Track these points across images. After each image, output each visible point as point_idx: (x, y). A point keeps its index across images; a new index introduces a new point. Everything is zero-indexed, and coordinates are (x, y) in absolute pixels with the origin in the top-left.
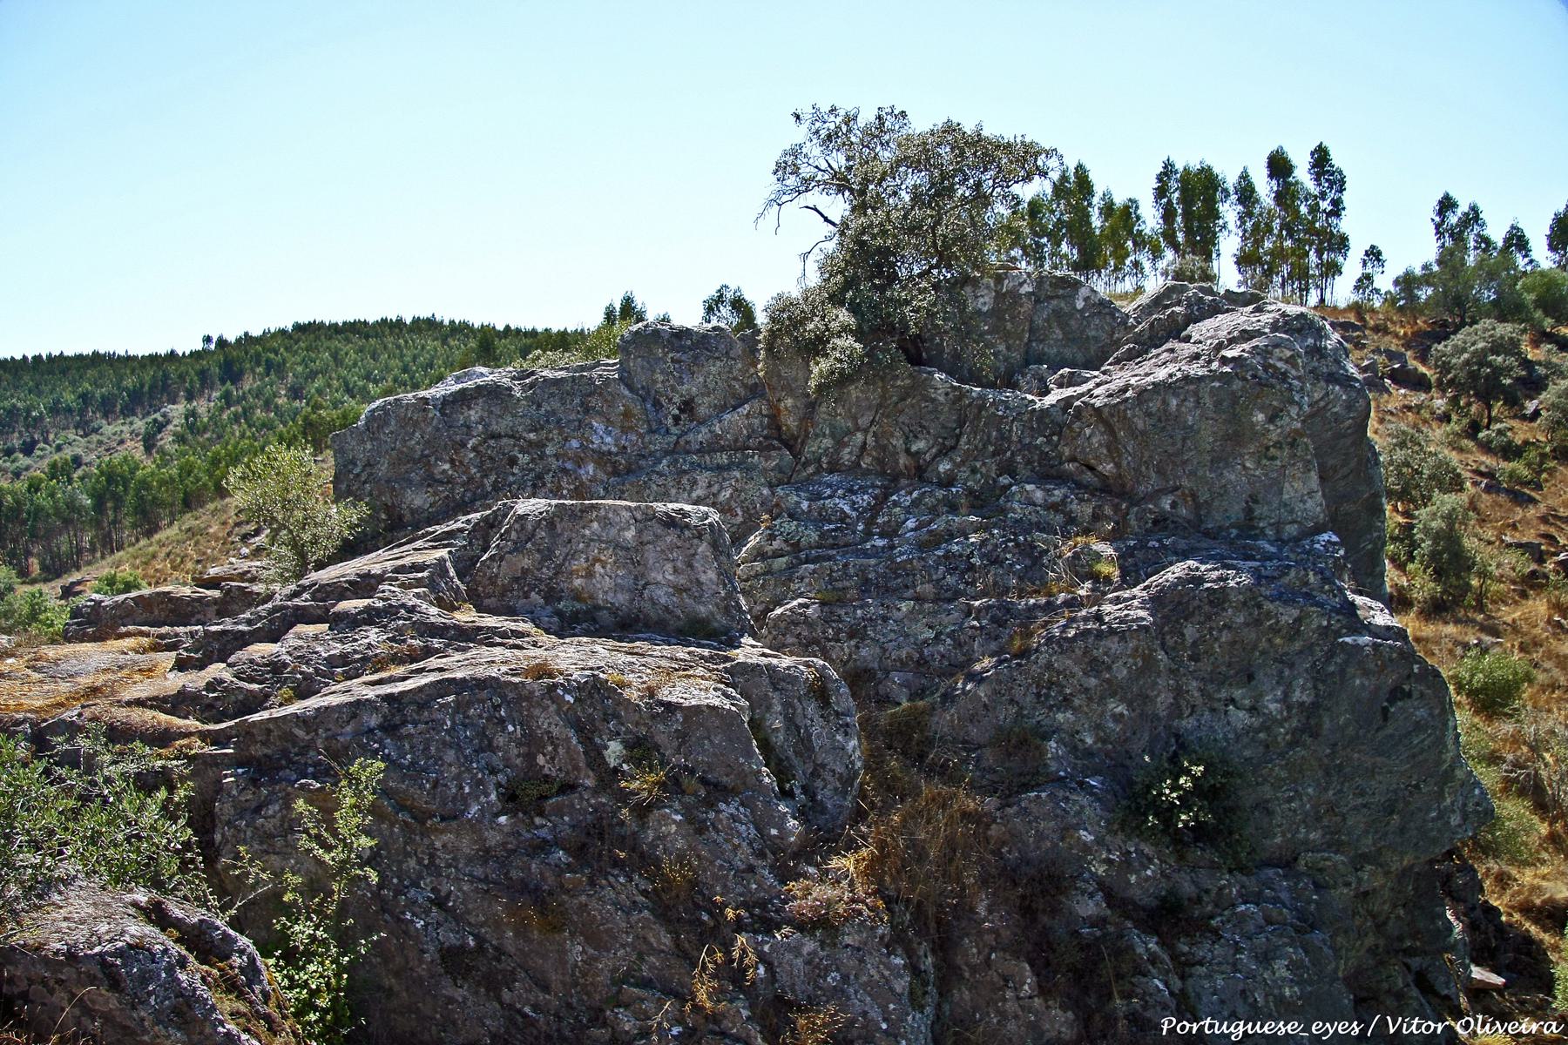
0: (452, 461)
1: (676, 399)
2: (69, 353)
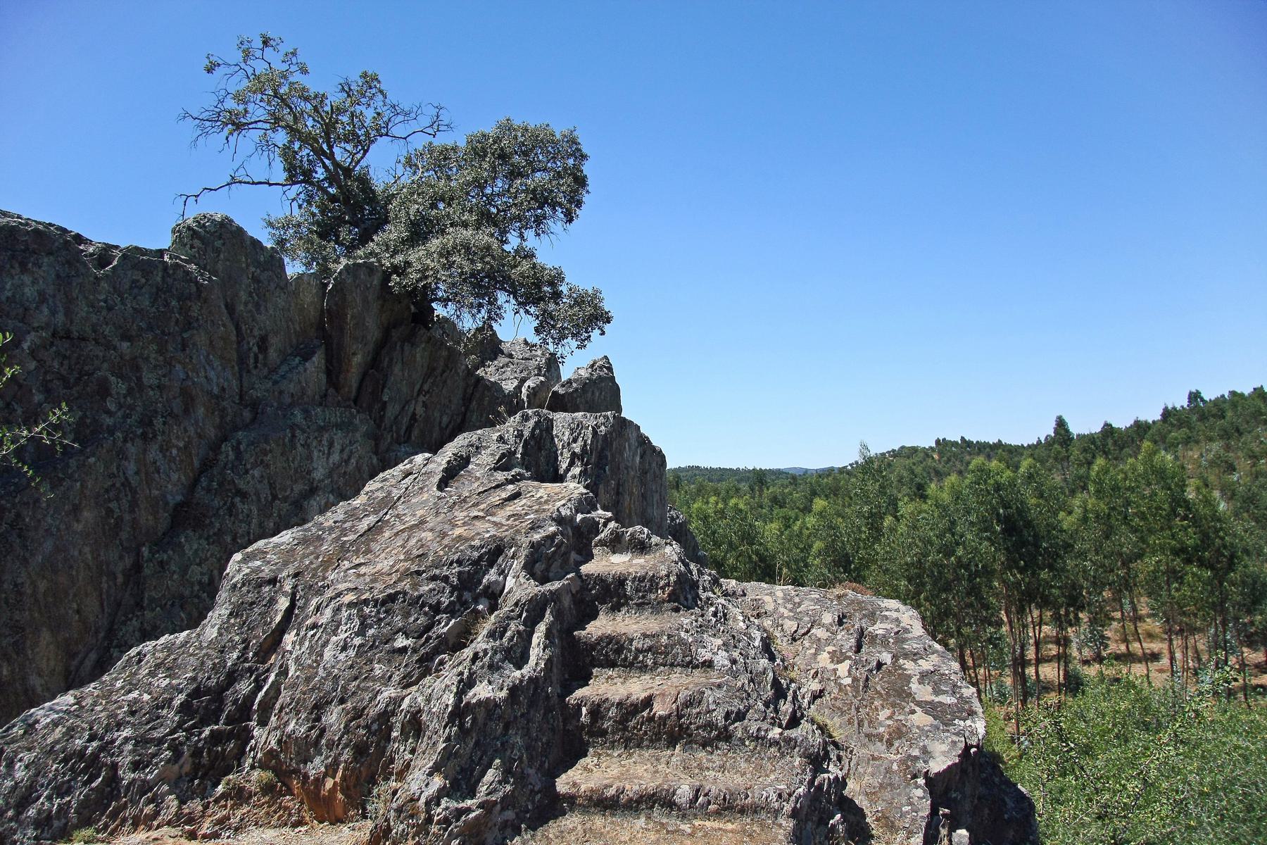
1: (256, 332)
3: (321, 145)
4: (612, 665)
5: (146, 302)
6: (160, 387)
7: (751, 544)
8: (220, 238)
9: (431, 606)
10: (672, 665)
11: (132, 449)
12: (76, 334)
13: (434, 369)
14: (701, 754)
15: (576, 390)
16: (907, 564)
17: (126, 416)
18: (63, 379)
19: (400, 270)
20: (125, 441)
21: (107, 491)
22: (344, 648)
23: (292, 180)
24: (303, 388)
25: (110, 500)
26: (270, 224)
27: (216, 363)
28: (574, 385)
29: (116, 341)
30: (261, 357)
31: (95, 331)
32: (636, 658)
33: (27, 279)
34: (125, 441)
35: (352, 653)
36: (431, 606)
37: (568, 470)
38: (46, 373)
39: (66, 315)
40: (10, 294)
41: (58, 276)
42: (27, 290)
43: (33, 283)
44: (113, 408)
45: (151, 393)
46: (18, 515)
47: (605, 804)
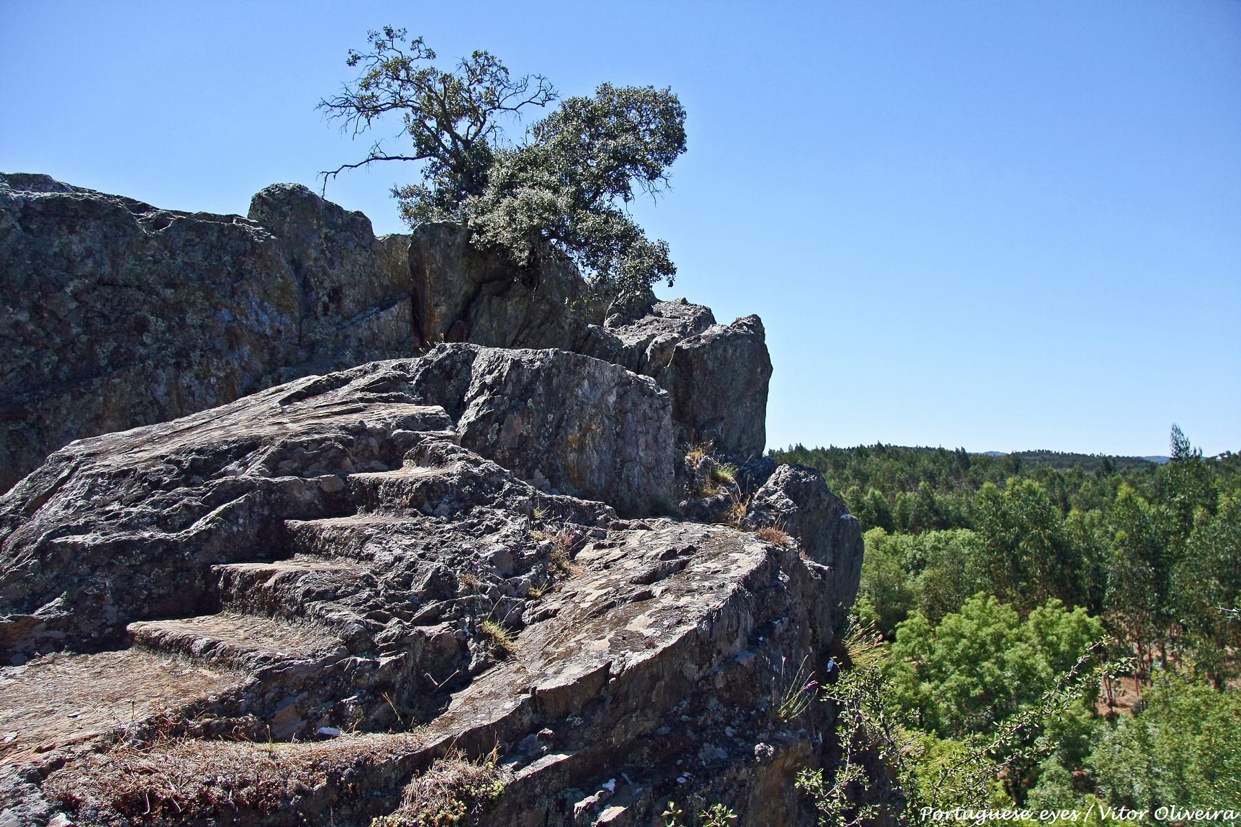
0: (36, 310)
1: (327, 284)
2: (1066, 452)
3: (446, 117)
4: (307, 551)
5: (198, 257)
6: (203, 327)
7: (1044, 528)
8: (288, 204)
9: (150, 483)
10: (347, 556)
11: (162, 375)
12: (121, 282)
13: (531, 322)
14: (285, 625)
15: (704, 345)
16: (1219, 560)
17: (160, 349)
18: (104, 316)
19: (480, 230)
20: (156, 367)
21: (133, 406)
22: (67, 507)
23: (421, 155)
24: (374, 334)
25: (136, 414)
26: (397, 193)
27: (271, 309)
28: (703, 341)
29: (159, 288)
30: (332, 306)
31: (138, 280)
32: (323, 546)
33: (75, 238)
34: (156, 367)
35: (71, 511)
36: (150, 483)
37: (473, 398)
38: (87, 312)
39: (112, 267)
40: (57, 250)
41: (105, 236)
42: (74, 247)
43: (80, 242)
44: (149, 341)
45: (193, 331)
46: (39, 418)
47: (153, 645)
